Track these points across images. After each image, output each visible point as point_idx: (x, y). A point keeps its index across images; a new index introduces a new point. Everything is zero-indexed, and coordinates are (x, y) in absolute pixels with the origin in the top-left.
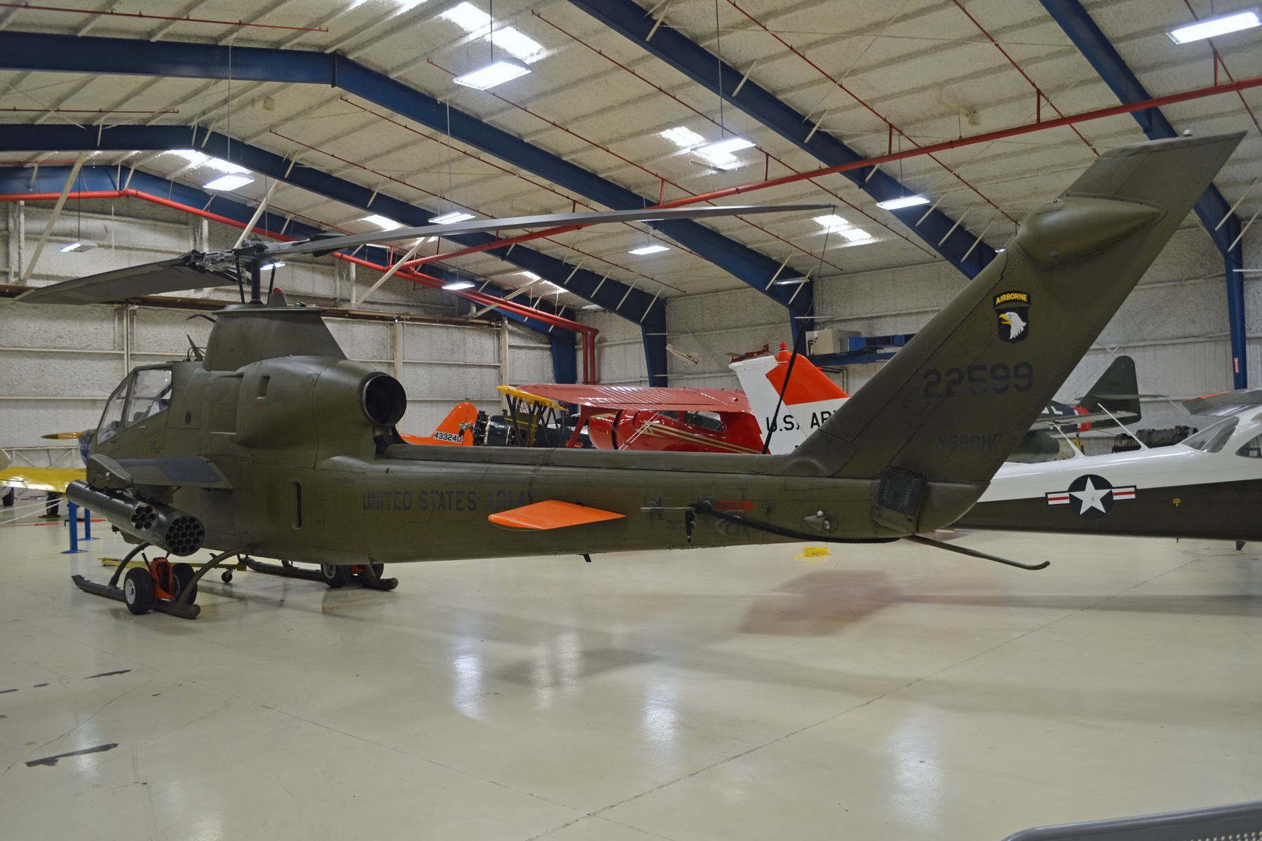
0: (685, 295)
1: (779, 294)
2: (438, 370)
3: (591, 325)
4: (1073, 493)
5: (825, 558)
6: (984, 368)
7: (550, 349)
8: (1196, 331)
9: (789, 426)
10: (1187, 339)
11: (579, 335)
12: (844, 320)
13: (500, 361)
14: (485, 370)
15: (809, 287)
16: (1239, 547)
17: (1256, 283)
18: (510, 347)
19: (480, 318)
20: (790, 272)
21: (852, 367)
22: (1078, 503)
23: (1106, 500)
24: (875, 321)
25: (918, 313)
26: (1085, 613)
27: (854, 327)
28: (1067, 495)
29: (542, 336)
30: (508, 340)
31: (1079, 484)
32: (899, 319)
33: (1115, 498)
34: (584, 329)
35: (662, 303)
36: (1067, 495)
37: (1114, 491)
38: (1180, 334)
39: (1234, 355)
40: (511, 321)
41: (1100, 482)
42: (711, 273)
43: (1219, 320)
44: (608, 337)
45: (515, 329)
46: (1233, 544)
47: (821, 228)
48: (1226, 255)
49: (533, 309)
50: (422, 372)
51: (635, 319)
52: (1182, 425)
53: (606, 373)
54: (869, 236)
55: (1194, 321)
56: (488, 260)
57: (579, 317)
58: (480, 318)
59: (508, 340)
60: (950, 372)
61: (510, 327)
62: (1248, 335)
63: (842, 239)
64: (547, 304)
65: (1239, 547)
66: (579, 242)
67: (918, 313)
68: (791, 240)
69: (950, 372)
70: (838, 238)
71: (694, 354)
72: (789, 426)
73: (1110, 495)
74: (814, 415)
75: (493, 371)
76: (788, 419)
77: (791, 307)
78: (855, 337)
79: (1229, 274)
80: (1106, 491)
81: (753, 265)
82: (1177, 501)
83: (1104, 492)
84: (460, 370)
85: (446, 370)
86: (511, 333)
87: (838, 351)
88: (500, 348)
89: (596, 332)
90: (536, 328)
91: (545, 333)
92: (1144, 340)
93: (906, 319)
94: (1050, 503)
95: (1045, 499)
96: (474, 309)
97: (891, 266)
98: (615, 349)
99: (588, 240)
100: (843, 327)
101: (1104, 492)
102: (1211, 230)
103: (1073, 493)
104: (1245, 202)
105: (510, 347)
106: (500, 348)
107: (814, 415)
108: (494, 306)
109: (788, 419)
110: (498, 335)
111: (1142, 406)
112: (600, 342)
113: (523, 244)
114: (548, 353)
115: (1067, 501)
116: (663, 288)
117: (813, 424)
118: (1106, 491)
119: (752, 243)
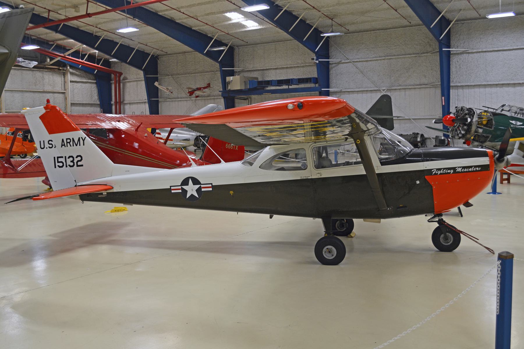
0: (167, 54)
1: (211, 55)
2: (27, 94)
3: (118, 71)
4: (184, 187)
5: (125, 213)
6: (62, 157)
7: (96, 83)
8: (426, 82)
9: (51, 146)
10: (421, 86)
11: (113, 76)
12: (250, 71)
13: (65, 90)
14: (56, 95)
15: (231, 50)
16: (271, 217)
17: (457, 56)
18: (71, 82)
19: (51, 65)
20: (218, 43)
21: (253, 97)
22: (185, 192)
23: (199, 191)
24: (265, 72)
25: (287, 68)
26: (177, 252)
27: (247, 75)
28: (180, 187)
29: (90, 76)
30: (69, 77)
31: (185, 182)
32: (278, 71)
33: (203, 190)
34: (115, 73)
35: (155, 59)
36: (180, 187)
37: (202, 186)
38: (418, 84)
39: (443, 95)
40: (71, 67)
41: (196, 181)
42: (174, 45)
43: (435, 77)
44: (128, 77)
45: (74, 71)
46: (268, 215)
47: (230, 19)
48: (440, 42)
49: (99, 66)
50: (17, 95)
51: (140, 68)
52: (416, 132)
53: (127, 98)
54: (257, 24)
55: (425, 76)
56: (49, 33)
57: (112, 65)
58: (51, 65)
59: (69, 77)
60: (77, 157)
61: (71, 70)
62: (452, 84)
63: (244, 26)
64: (91, 58)
65: (271, 217)
66: (99, 24)
67: (287, 68)
68: (215, 26)
69: (77, 157)
70: (239, 25)
71: (170, 88)
72: (51, 146)
73: (200, 188)
74: (63, 140)
75: (61, 96)
76: (50, 142)
77: (220, 63)
78: (252, 81)
79: (441, 51)
80: (198, 186)
81: (196, 39)
82: (231, 192)
83: (197, 186)
84: (41, 94)
85: (32, 94)
86: (72, 74)
87: (243, 88)
88: (65, 82)
89: (121, 74)
90: (87, 71)
91: (93, 74)
92: (400, 85)
93: (281, 71)
94: (173, 191)
95: (170, 189)
96: (48, 60)
97: (274, 41)
98: (132, 83)
99: (104, 22)
100: (247, 75)
101: (197, 186)
102: (428, 27)
103: (184, 187)
104: (446, 12)
105: (71, 82)
106: (65, 82)
107: (63, 140)
108: (59, 58)
109: (50, 142)
110: (64, 75)
111: (394, 121)
112: (124, 79)
113: (66, 23)
114: (95, 85)
115: (180, 191)
116: (154, 50)
117: (62, 145)
118: (198, 186)
119: (195, 26)
